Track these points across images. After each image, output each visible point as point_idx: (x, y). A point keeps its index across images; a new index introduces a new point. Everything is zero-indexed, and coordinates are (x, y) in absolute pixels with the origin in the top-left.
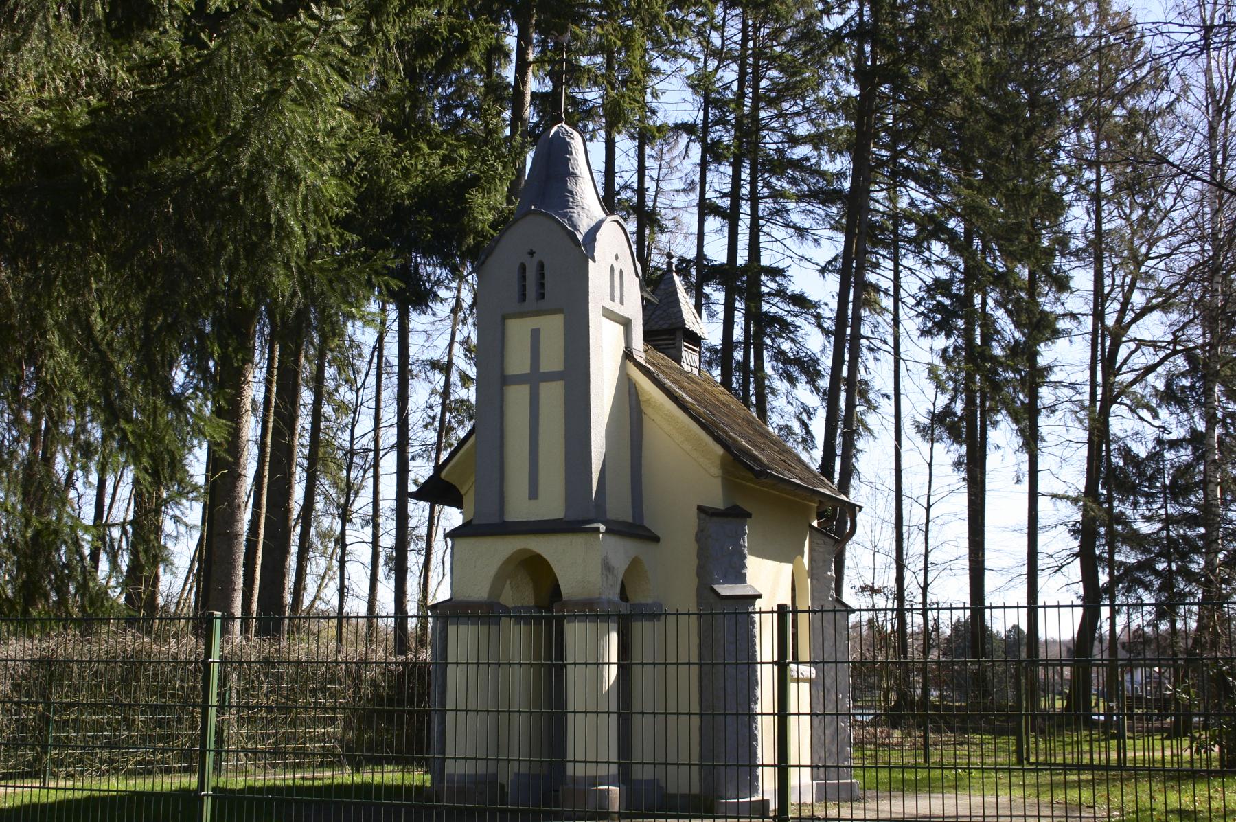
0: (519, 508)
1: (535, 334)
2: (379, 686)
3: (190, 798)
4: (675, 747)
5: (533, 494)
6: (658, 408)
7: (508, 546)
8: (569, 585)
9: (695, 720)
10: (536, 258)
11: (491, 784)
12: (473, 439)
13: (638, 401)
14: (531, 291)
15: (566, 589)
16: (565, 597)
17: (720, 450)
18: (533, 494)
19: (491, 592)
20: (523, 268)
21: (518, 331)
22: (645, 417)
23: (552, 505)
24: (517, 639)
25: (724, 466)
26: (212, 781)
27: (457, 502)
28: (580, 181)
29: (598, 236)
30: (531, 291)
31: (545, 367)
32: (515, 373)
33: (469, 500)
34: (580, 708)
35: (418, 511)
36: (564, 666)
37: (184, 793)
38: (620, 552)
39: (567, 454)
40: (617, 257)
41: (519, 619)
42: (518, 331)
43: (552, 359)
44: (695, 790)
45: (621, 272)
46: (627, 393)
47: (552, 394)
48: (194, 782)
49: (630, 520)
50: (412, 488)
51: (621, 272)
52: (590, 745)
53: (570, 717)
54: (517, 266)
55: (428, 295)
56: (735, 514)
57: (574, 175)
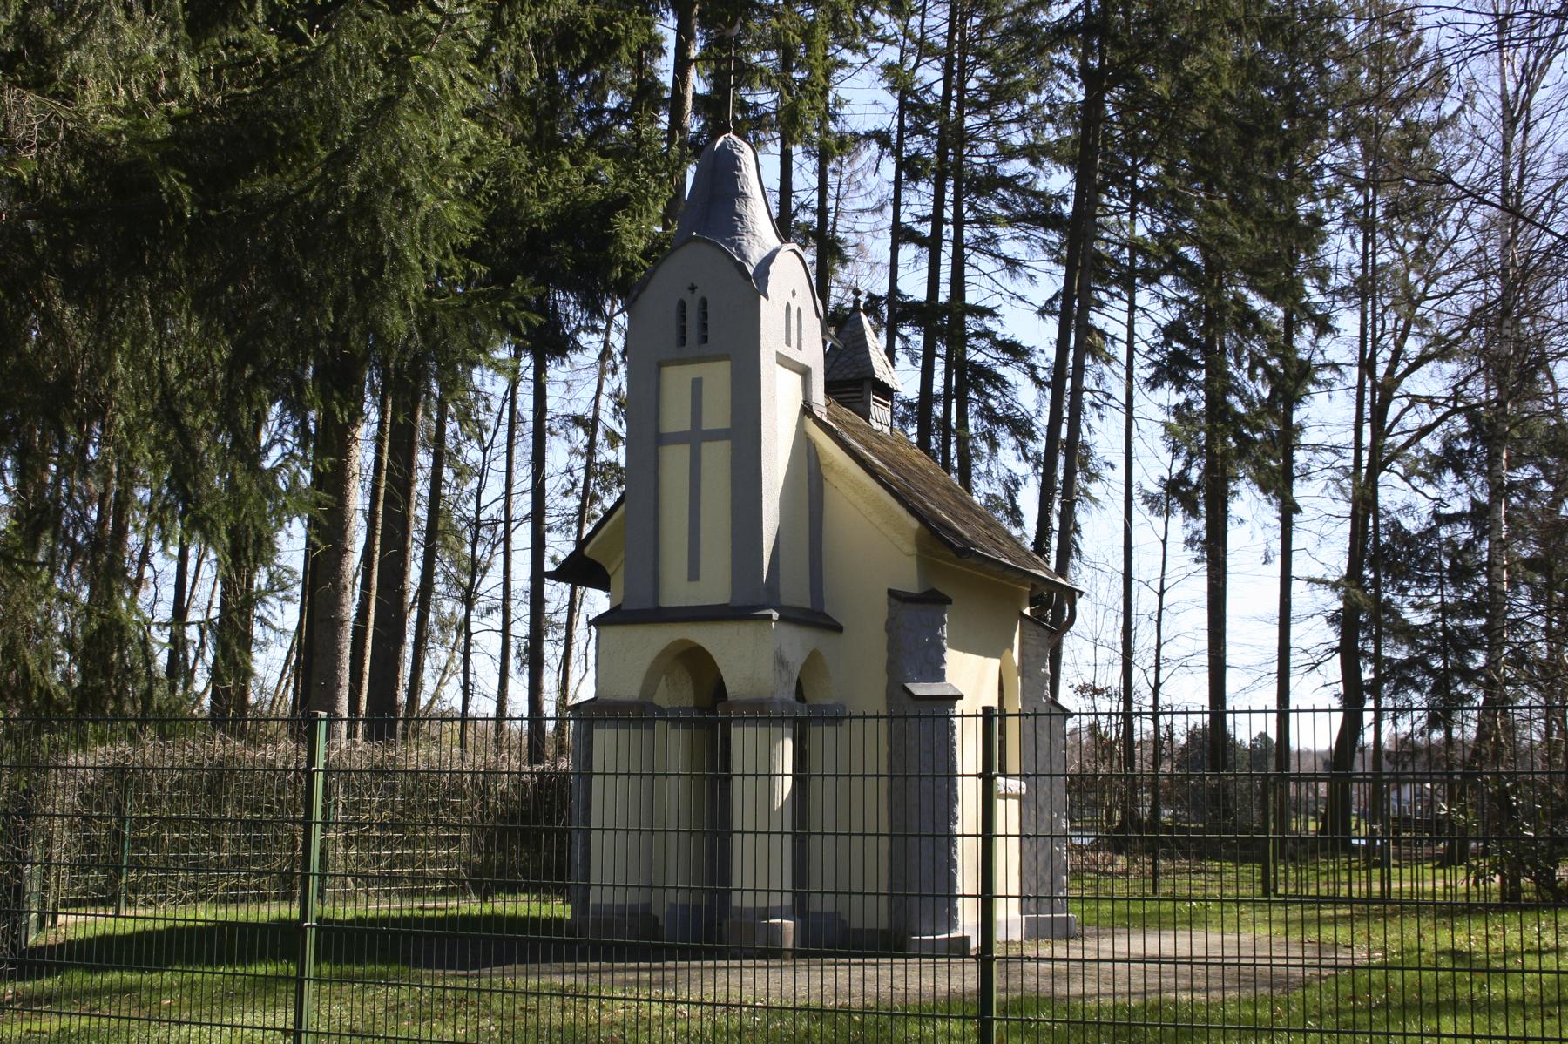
0: (677, 591)
1: (697, 384)
5: (694, 575)
8: (736, 682)
10: (698, 294)
13: (818, 465)
15: (733, 687)
16: (730, 697)
17: (914, 524)
18: (694, 575)
19: (643, 691)
20: (682, 306)
21: (677, 380)
23: (715, 588)
26: (316, 909)
27: (604, 585)
28: (751, 203)
31: (708, 423)
32: (673, 430)
33: (617, 581)
35: (557, 594)
37: (283, 925)
38: (795, 643)
40: (794, 294)
42: (677, 380)
43: (717, 414)
44: (884, 925)
45: (799, 311)
47: (717, 456)
48: (296, 913)
49: (808, 606)
50: (549, 567)
51: (799, 311)
56: (932, 600)
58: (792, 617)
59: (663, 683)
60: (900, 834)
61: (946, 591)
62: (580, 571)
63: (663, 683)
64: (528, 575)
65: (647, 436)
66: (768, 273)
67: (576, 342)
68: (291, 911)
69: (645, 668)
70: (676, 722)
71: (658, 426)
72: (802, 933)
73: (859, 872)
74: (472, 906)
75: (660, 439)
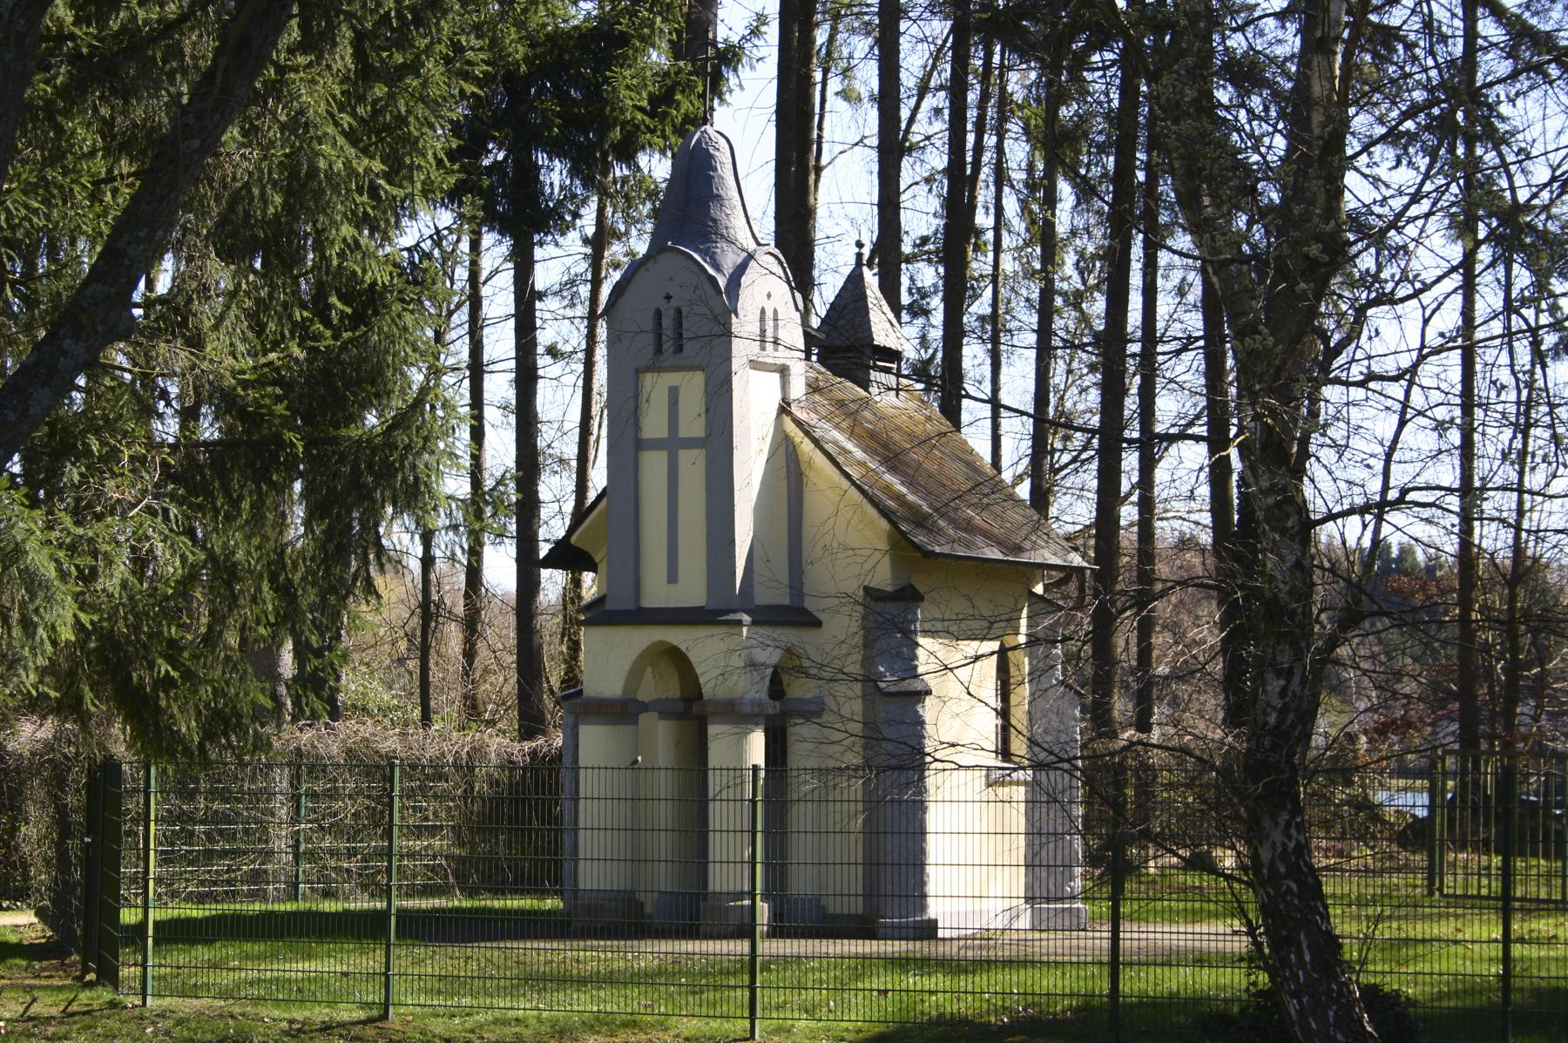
0: (657, 594)
1: (674, 393)
5: (673, 578)
7: (641, 638)
9: (860, 868)
10: (673, 303)
12: (604, 502)
13: (797, 463)
14: (668, 345)
15: (707, 690)
16: (706, 696)
17: (884, 524)
18: (673, 578)
20: (658, 314)
21: (656, 386)
23: (692, 591)
25: (890, 536)
26: (396, 903)
27: (593, 567)
30: (668, 345)
31: (684, 432)
33: (602, 568)
35: (553, 582)
36: (707, 832)
39: (709, 579)
40: (769, 296)
43: (692, 425)
44: (860, 911)
45: (775, 311)
46: (787, 467)
47: (692, 464)
49: (786, 601)
50: (544, 550)
51: (775, 311)
54: (651, 314)
56: (908, 596)
58: (767, 617)
59: (649, 670)
62: (569, 556)
63: (649, 670)
64: (541, 384)
65: (628, 448)
66: (739, 285)
68: (380, 905)
69: (627, 668)
70: (663, 715)
72: (776, 915)
73: (829, 858)
75: (640, 445)
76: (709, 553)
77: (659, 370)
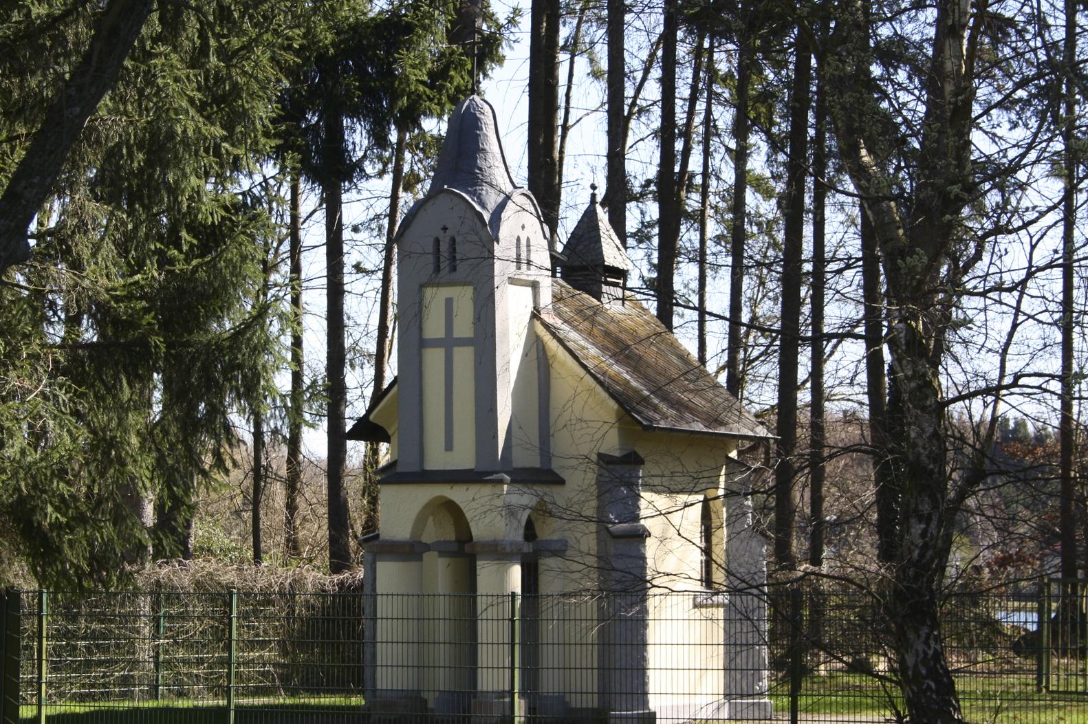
0: (437, 459)
1: (449, 302)
2: (313, 607)
3: (222, 712)
4: (573, 673)
5: (449, 447)
6: (563, 364)
8: (479, 530)
11: (415, 698)
12: (395, 389)
15: (475, 532)
16: (475, 539)
17: (613, 405)
18: (449, 447)
19: (413, 533)
21: (436, 298)
22: (552, 371)
23: (464, 457)
24: (439, 571)
26: (234, 701)
28: (490, 156)
29: (503, 215)
30: (445, 265)
32: (432, 337)
33: (394, 439)
34: (485, 641)
37: (218, 709)
38: (524, 498)
40: (523, 227)
41: (442, 554)
42: (436, 298)
43: (464, 327)
44: (596, 705)
45: (528, 239)
47: (464, 358)
48: (225, 702)
49: (538, 465)
51: (528, 239)
52: (496, 671)
53: (479, 646)
55: (353, 170)
57: (484, 150)
60: (605, 643)
61: (642, 454)
63: (431, 518)
67: (362, 170)
68: (222, 702)
71: (421, 329)
74: (282, 700)
75: (423, 343)
76: (476, 418)
77: (438, 285)
